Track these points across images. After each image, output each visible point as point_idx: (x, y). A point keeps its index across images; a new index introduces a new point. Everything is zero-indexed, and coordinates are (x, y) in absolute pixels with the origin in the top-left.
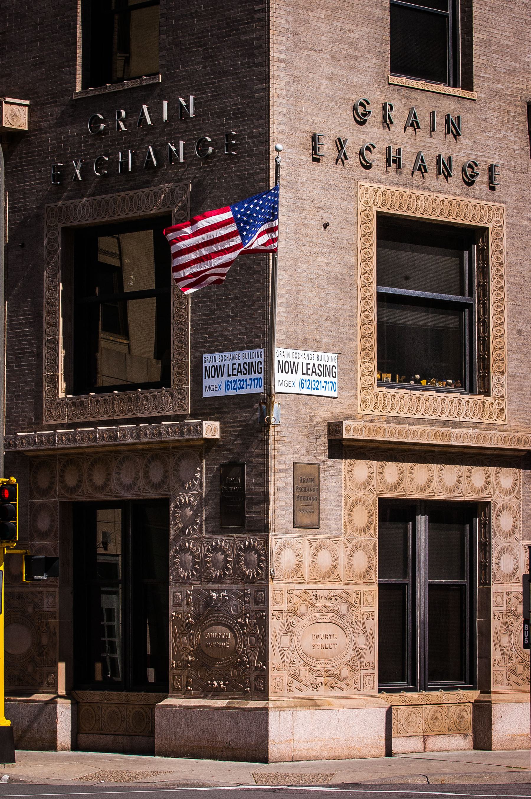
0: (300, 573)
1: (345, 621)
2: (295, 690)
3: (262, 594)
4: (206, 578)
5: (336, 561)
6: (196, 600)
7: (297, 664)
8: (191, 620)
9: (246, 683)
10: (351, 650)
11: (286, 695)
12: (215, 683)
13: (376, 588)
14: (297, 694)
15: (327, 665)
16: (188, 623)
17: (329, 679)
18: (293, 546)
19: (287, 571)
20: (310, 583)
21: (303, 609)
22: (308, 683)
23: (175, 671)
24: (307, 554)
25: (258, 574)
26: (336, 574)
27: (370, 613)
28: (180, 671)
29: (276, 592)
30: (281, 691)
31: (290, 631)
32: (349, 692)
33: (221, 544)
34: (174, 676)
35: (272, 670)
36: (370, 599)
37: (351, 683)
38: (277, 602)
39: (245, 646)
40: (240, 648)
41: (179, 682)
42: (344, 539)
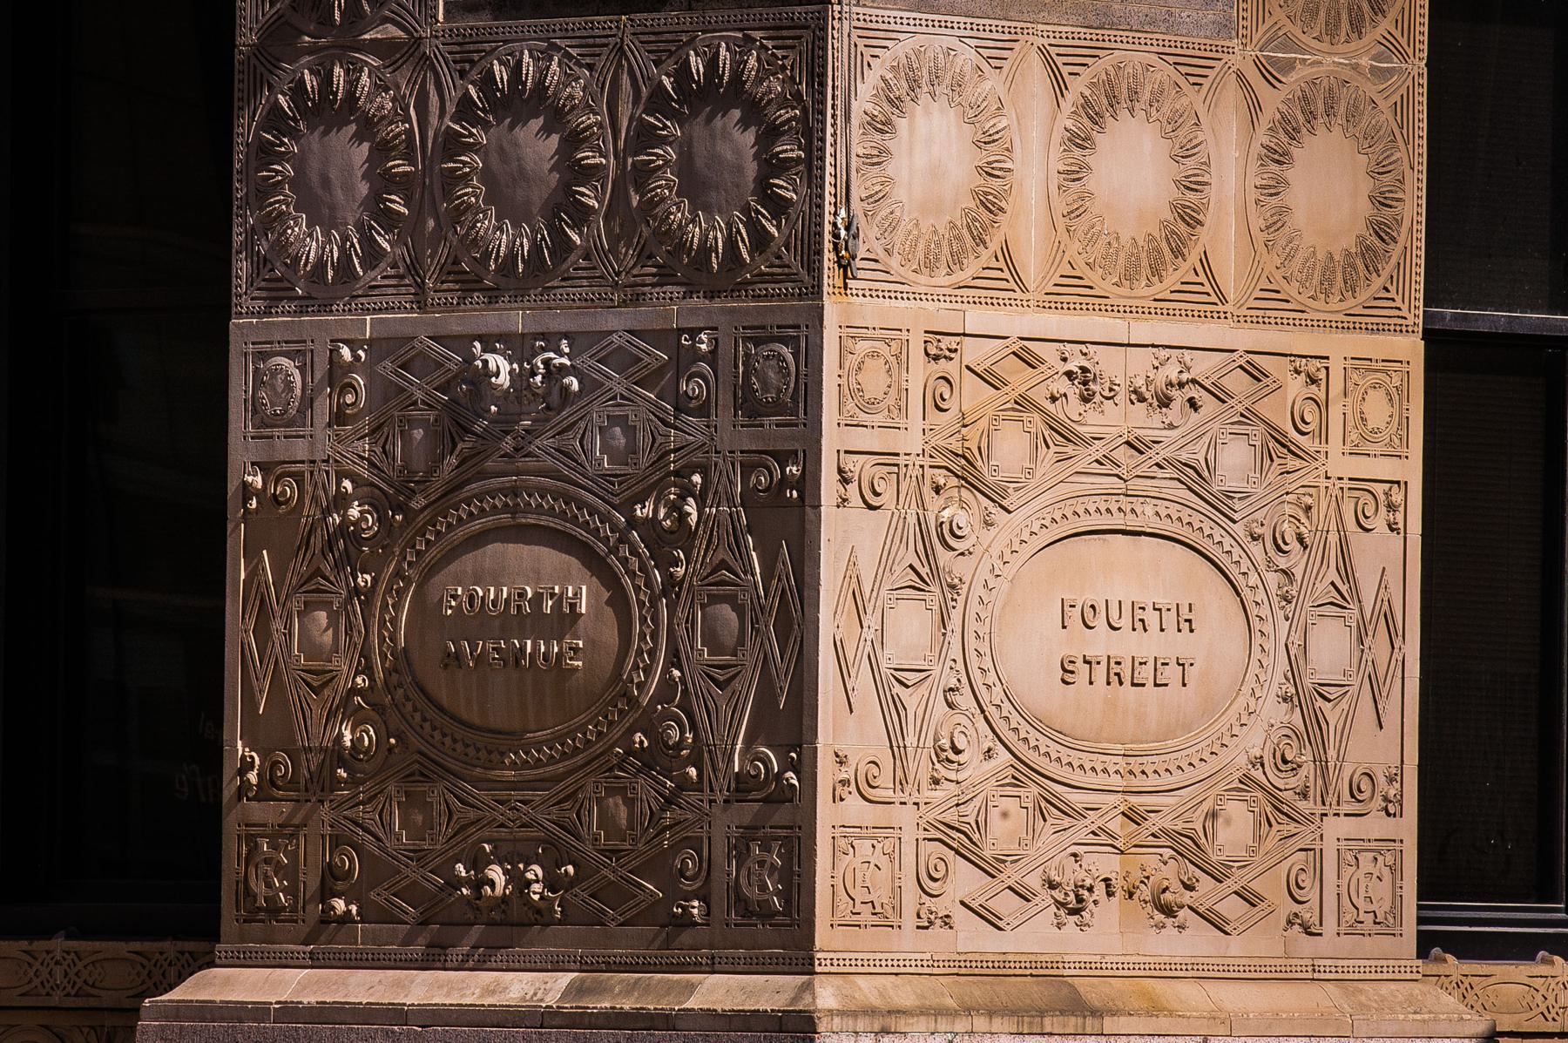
0: (994, 246)
1: (1239, 529)
2: (960, 915)
3: (780, 358)
4: (451, 270)
5: (1193, 185)
6: (388, 394)
7: (974, 768)
8: (354, 512)
9: (682, 873)
10: (1272, 698)
11: (908, 943)
12: (496, 873)
13: (1411, 348)
14: (972, 938)
15: (1139, 782)
16: (342, 529)
17: (1151, 861)
18: (957, 85)
19: (925, 227)
20: (1054, 301)
21: (1010, 450)
22: (1034, 882)
23: (259, 811)
24: (1036, 134)
25: (760, 240)
26: (1193, 258)
27: (1379, 489)
28: (286, 807)
29: (863, 347)
30: (885, 919)
31: (935, 571)
32: (1256, 942)
33: (542, 73)
34: (252, 841)
35: (837, 798)
36: (1378, 410)
37: (1270, 886)
38: (869, 406)
39: (674, 659)
40: (648, 670)
41: (279, 868)
42: (1241, 57)
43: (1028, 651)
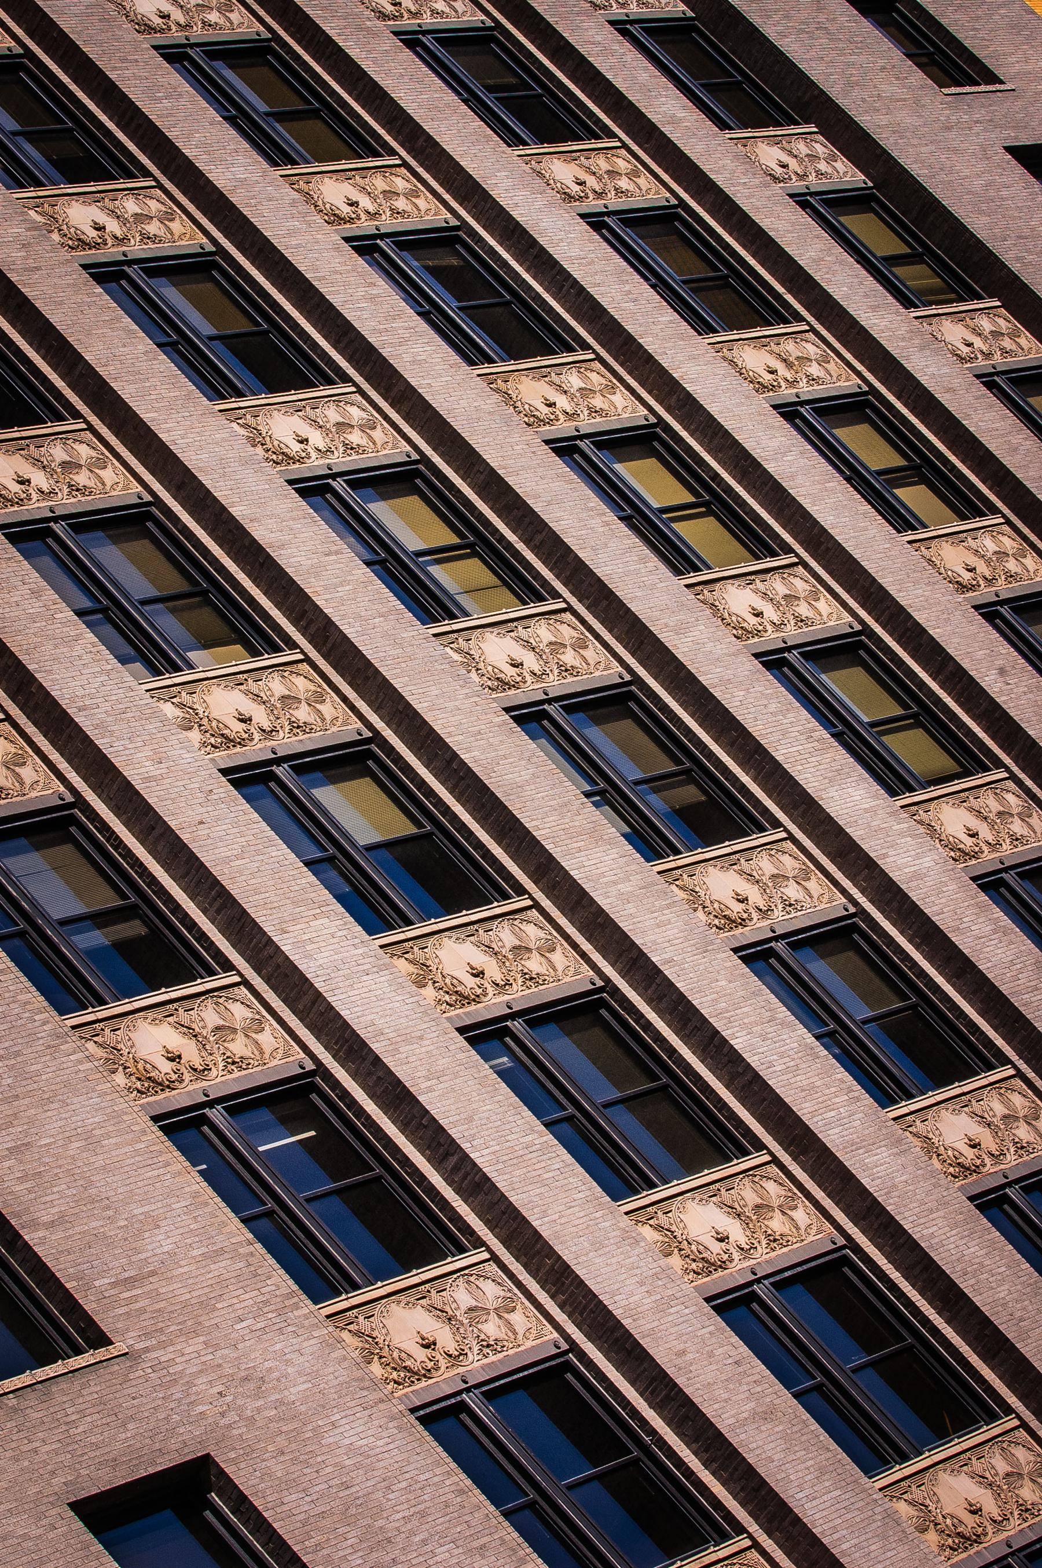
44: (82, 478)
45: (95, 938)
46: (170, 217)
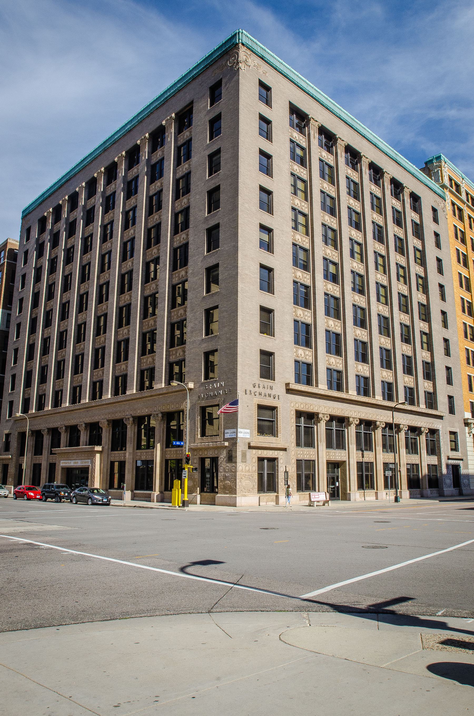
21: (243, 478)
43: (244, 484)
44: (332, 224)
45: (302, 262)
46: (306, 208)
